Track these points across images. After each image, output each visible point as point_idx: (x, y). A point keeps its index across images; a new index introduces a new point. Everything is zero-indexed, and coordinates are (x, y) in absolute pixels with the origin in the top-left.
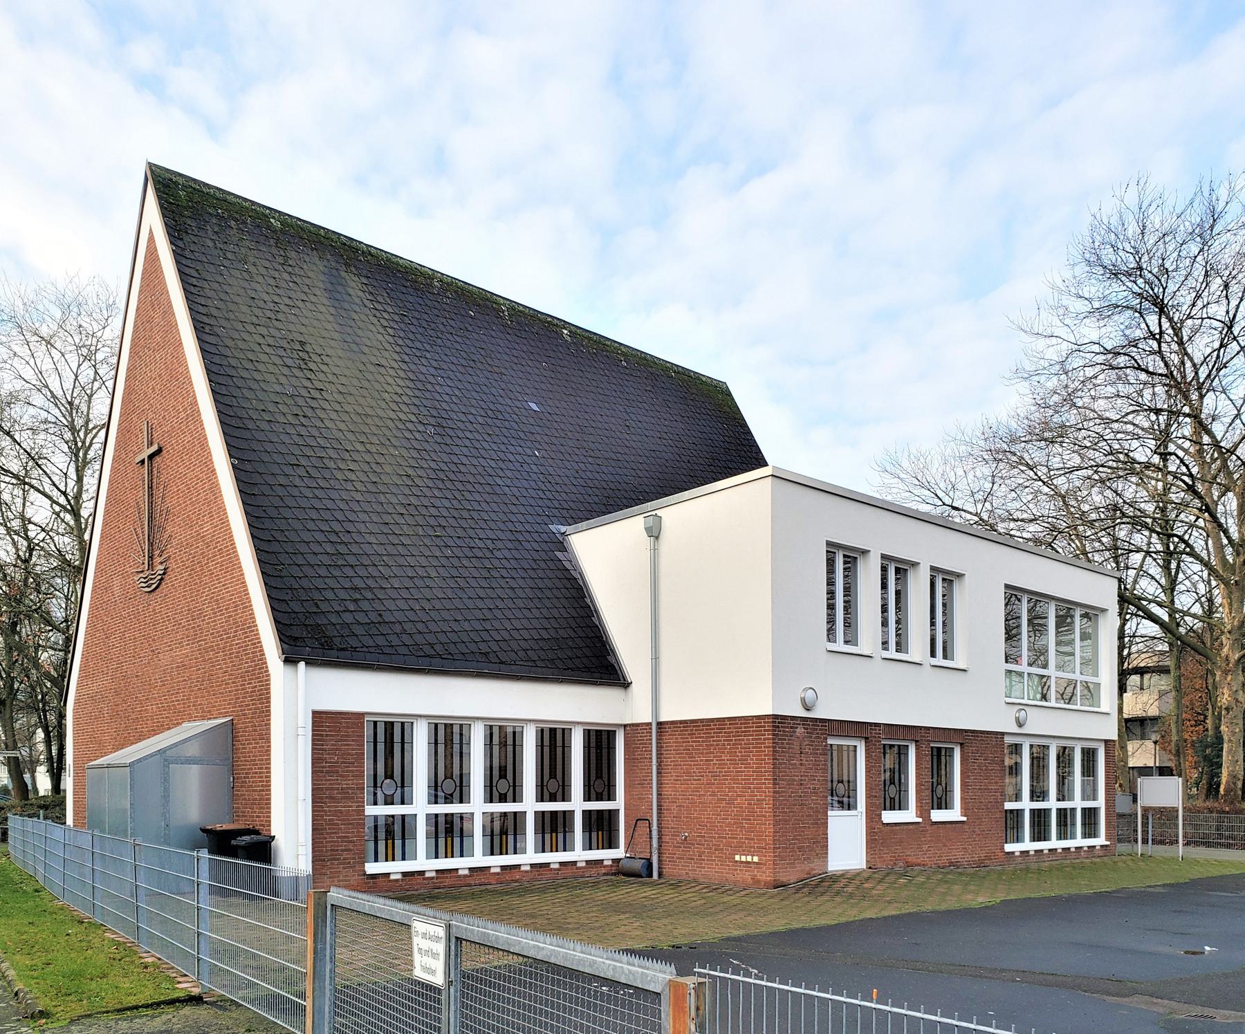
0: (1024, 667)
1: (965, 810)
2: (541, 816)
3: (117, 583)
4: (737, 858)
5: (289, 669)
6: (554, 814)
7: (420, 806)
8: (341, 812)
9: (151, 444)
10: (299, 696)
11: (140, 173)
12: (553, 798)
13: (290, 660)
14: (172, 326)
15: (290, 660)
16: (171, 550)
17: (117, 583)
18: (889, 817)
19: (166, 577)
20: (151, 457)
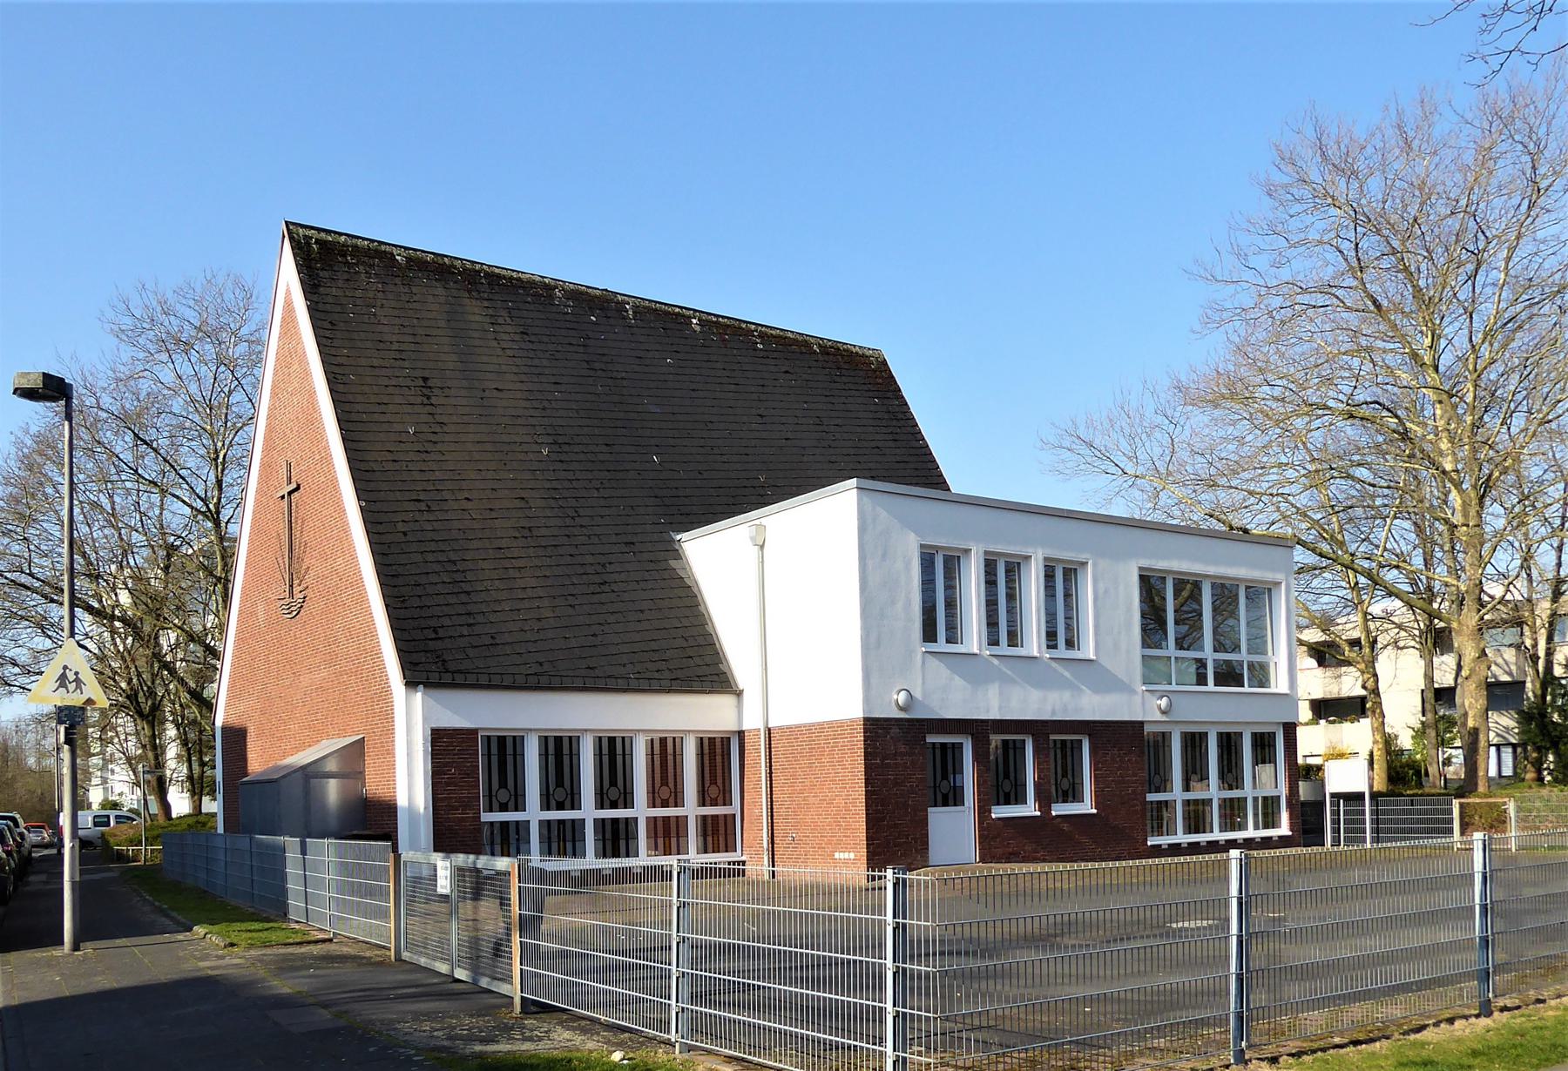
0: (1171, 649)
2: (653, 821)
3: (261, 608)
4: (837, 855)
6: (666, 819)
7: (534, 813)
12: (665, 804)
13: (411, 684)
14: (307, 374)
16: (308, 580)
17: (261, 608)
18: (999, 812)
20: (290, 493)
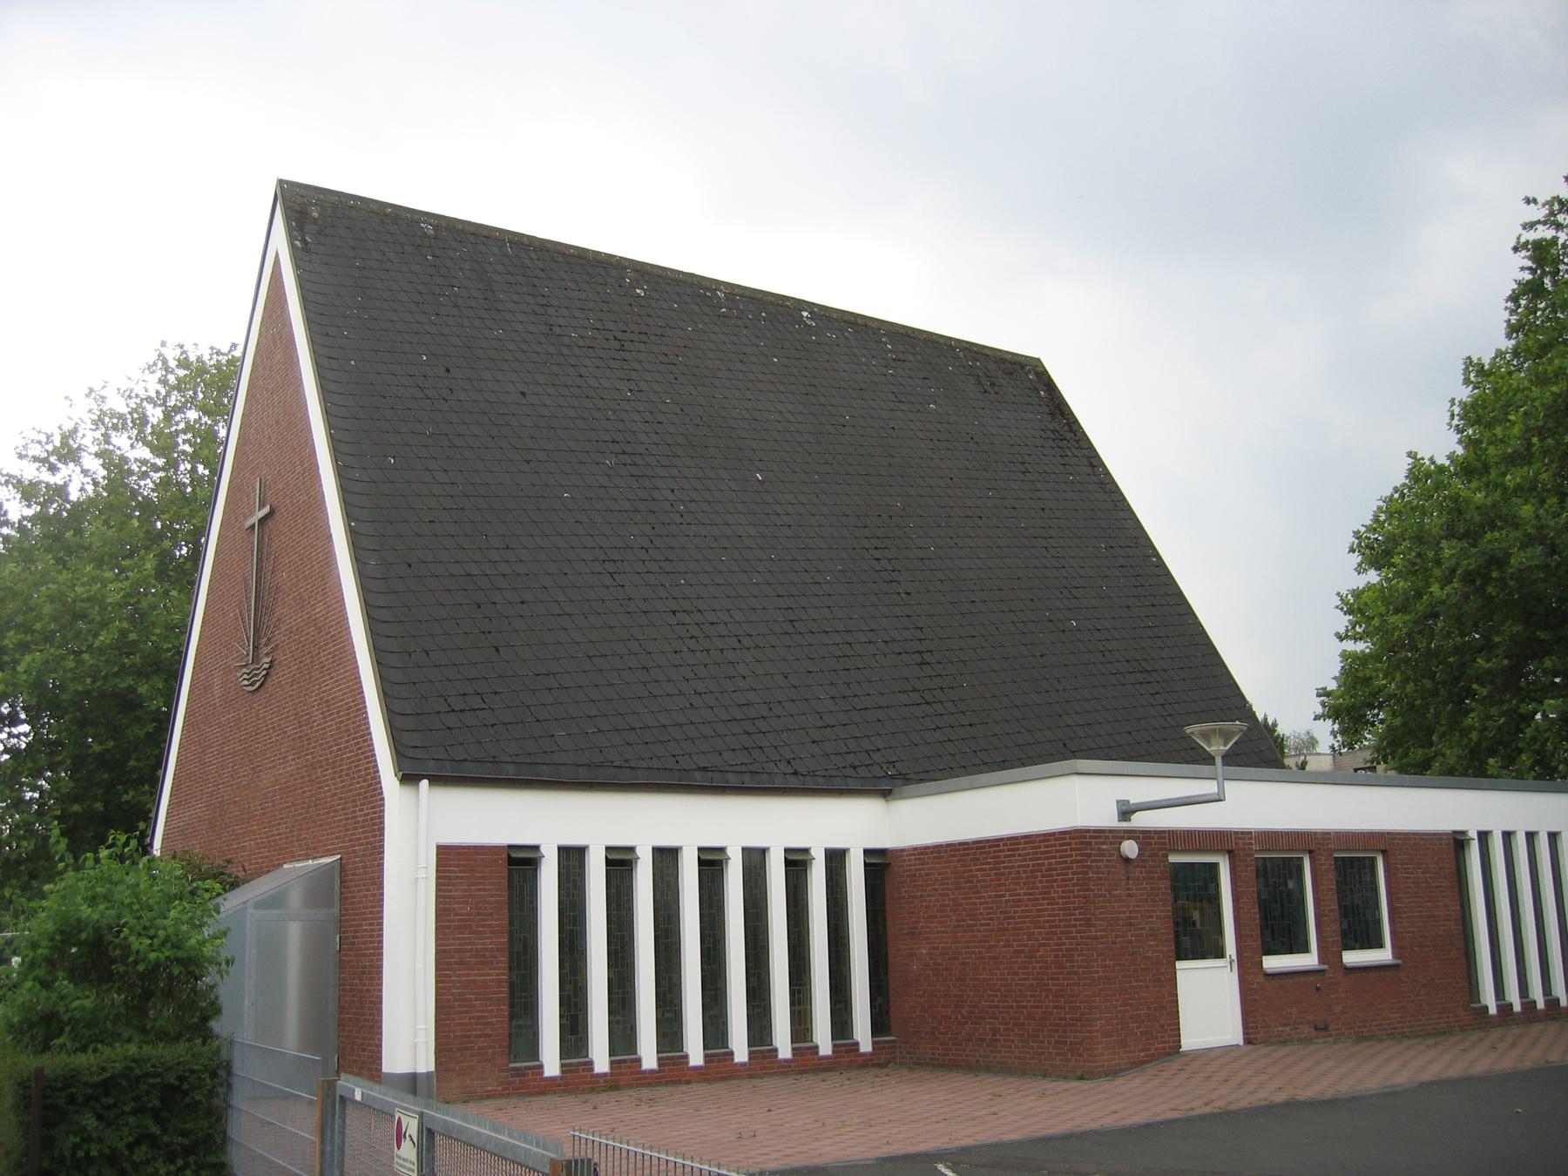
1: (1322, 959)
5: (408, 791)
8: (474, 981)
9: (262, 506)
10: (422, 825)
11: (270, 190)
15: (408, 778)
19: (273, 672)
20: (262, 521)
